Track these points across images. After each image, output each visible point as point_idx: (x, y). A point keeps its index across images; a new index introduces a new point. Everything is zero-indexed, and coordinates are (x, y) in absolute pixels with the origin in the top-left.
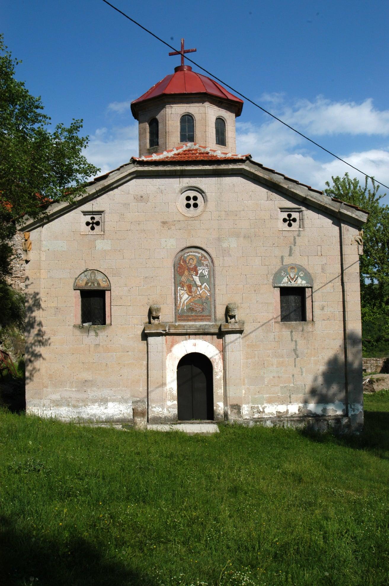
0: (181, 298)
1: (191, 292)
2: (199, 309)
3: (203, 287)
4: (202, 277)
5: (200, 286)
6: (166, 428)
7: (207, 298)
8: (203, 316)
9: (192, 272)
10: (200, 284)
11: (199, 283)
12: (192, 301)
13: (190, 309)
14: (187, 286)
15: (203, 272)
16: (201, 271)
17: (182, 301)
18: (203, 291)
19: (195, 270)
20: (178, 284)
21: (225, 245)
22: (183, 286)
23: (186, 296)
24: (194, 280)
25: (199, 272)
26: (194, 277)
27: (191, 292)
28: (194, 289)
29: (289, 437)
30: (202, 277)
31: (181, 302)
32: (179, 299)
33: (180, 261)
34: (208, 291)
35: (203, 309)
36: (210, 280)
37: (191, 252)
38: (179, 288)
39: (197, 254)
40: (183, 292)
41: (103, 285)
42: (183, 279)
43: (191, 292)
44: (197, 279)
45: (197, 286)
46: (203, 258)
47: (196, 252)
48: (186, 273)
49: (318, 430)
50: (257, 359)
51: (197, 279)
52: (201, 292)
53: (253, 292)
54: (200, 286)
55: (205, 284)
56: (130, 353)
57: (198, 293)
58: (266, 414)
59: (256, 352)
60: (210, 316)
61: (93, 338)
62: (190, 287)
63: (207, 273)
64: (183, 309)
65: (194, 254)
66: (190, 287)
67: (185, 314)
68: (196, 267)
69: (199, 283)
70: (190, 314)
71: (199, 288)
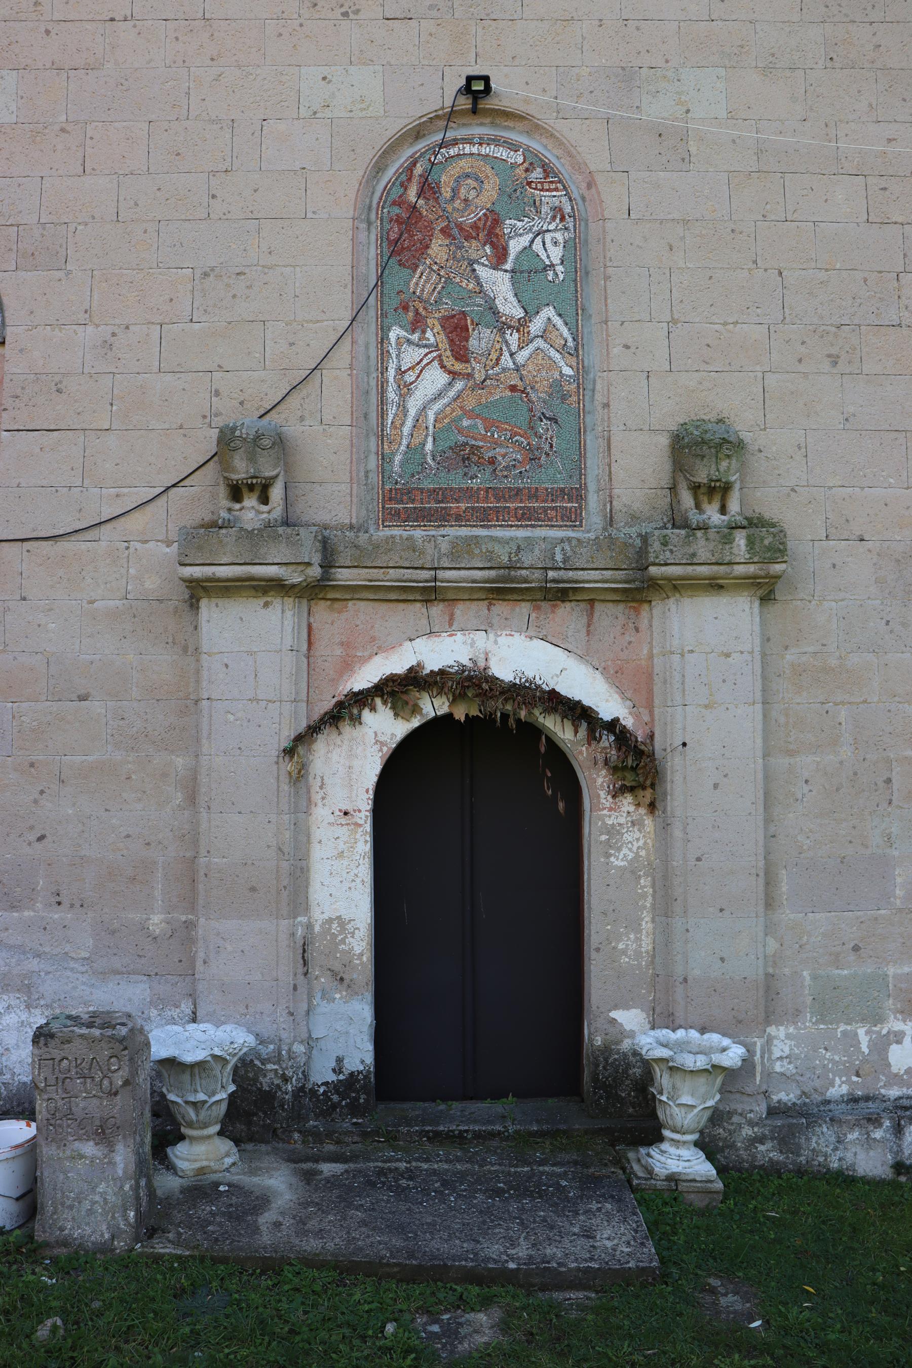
0: (405, 390)
1: (462, 355)
2: (506, 455)
3: (536, 326)
4: (528, 273)
6: (452, 394)
7: (557, 389)
8: (534, 495)
10: (519, 313)
11: (511, 308)
12: (470, 403)
13: (457, 448)
15: (537, 246)
16: (525, 240)
17: (413, 405)
18: (535, 352)
19: (491, 232)
20: (387, 300)
21: (657, 109)
22: (418, 324)
23: (434, 379)
24: (480, 290)
25: (515, 246)
26: (484, 272)
28: (480, 340)
30: (528, 273)
31: (403, 410)
33: (405, 187)
36: (573, 289)
37: (469, 141)
38: (395, 333)
39: (502, 153)
40: (412, 355)
42: (422, 282)
43: (462, 355)
44: (499, 284)
45: (503, 326)
46: (537, 174)
47: (496, 141)
48: (438, 249)
49: (833, 1126)
50: (846, 752)
51: (499, 284)
52: (522, 356)
53: (826, 366)
54: (521, 326)
55: (549, 312)
56: (96, 707)
57: (506, 361)
58: (896, 1080)
59: (843, 714)
61: (340, 1053)
62: (457, 330)
63: (556, 254)
65: (485, 150)
66: (457, 330)
67: (428, 484)
68: (497, 222)
69: (511, 308)
70: (456, 480)
71: (513, 338)
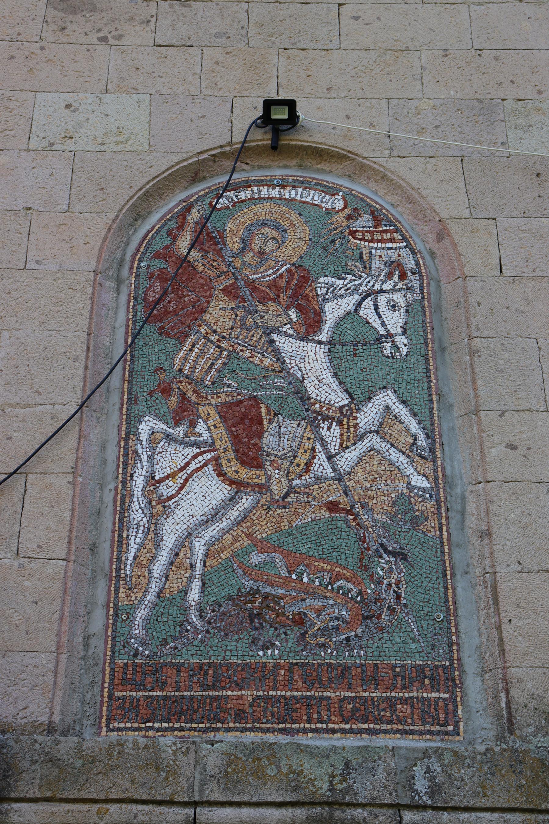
0: (160, 507)
1: (251, 457)
2: (326, 609)
3: (368, 416)
4: (353, 347)
5: (344, 417)
8: (371, 678)
9: (271, 315)
10: (340, 399)
11: (326, 391)
12: (264, 529)
13: (241, 598)
14: (226, 411)
17: (171, 533)
18: (370, 452)
19: (299, 294)
22: (185, 413)
23: (207, 492)
25: (333, 311)
26: (286, 345)
27: (250, 455)
28: (280, 436)
29: (102, 570)
30: (353, 347)
32: (137, 514)
34: (411, 450)
35: (367, 613)
41: (261, 100)
42: (193, 357)
45: (314, 416)
46: (364, 221)
48: (219, 313)
51: (311, 363)
54: (344, 417)
57: (322, 466)
60: (448, 678)
62: (245, 423)
63: (394, 321)
64: (170, 603)
66: (245, 423)
67: (189, 658)
69: (326, 391)
70: (238, 651)
71: (332, 435)
